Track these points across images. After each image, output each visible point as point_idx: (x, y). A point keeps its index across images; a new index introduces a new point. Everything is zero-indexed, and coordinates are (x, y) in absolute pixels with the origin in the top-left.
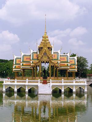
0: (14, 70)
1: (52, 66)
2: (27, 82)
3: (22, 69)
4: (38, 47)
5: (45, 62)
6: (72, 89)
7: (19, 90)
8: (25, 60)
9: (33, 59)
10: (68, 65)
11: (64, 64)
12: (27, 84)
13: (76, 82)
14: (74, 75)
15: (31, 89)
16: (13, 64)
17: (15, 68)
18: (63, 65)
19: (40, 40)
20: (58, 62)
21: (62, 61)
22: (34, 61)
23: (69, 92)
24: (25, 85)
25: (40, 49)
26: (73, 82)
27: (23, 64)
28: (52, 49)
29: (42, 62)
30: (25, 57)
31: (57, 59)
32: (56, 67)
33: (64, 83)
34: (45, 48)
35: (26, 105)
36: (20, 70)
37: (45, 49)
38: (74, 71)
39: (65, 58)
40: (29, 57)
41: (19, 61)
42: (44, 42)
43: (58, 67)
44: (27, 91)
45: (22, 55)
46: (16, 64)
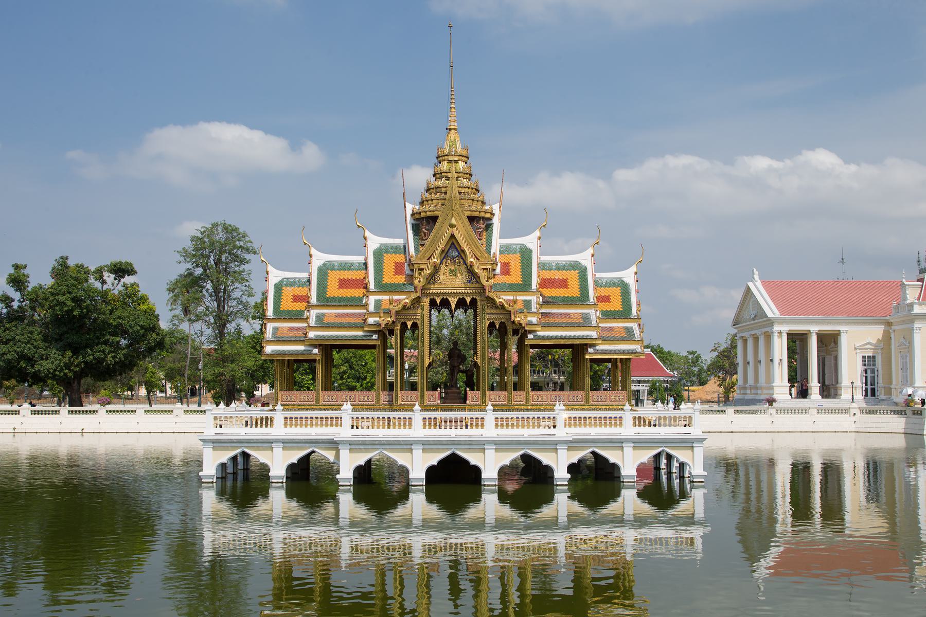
0: (269, 349)
2: (347, 422)
3: (375, 332)
4: (409, 212)
5: (453, 301)
7: (363, 474)
8: (333, 291)
11: (567, 315)
12: (344, 432)
13: (639, 421)
15: (369, 462)
18: (564, 320)
20: (528, 304)
21: (549, 292)
22: (386, 298)
23: (453, 480)
24: (336, 443)
25: (424, 224)
27: (319, 318)
28: (489, 227)
29: (433, 303)
30: (389, 262)
32: (515, 332)
33: (568, 430)
34: (454, 221)
35: (338, 562)
36: (361, 333)
39: (573, 277)
41: (297, 299)
43: (531, 332)
44: (350, 475)
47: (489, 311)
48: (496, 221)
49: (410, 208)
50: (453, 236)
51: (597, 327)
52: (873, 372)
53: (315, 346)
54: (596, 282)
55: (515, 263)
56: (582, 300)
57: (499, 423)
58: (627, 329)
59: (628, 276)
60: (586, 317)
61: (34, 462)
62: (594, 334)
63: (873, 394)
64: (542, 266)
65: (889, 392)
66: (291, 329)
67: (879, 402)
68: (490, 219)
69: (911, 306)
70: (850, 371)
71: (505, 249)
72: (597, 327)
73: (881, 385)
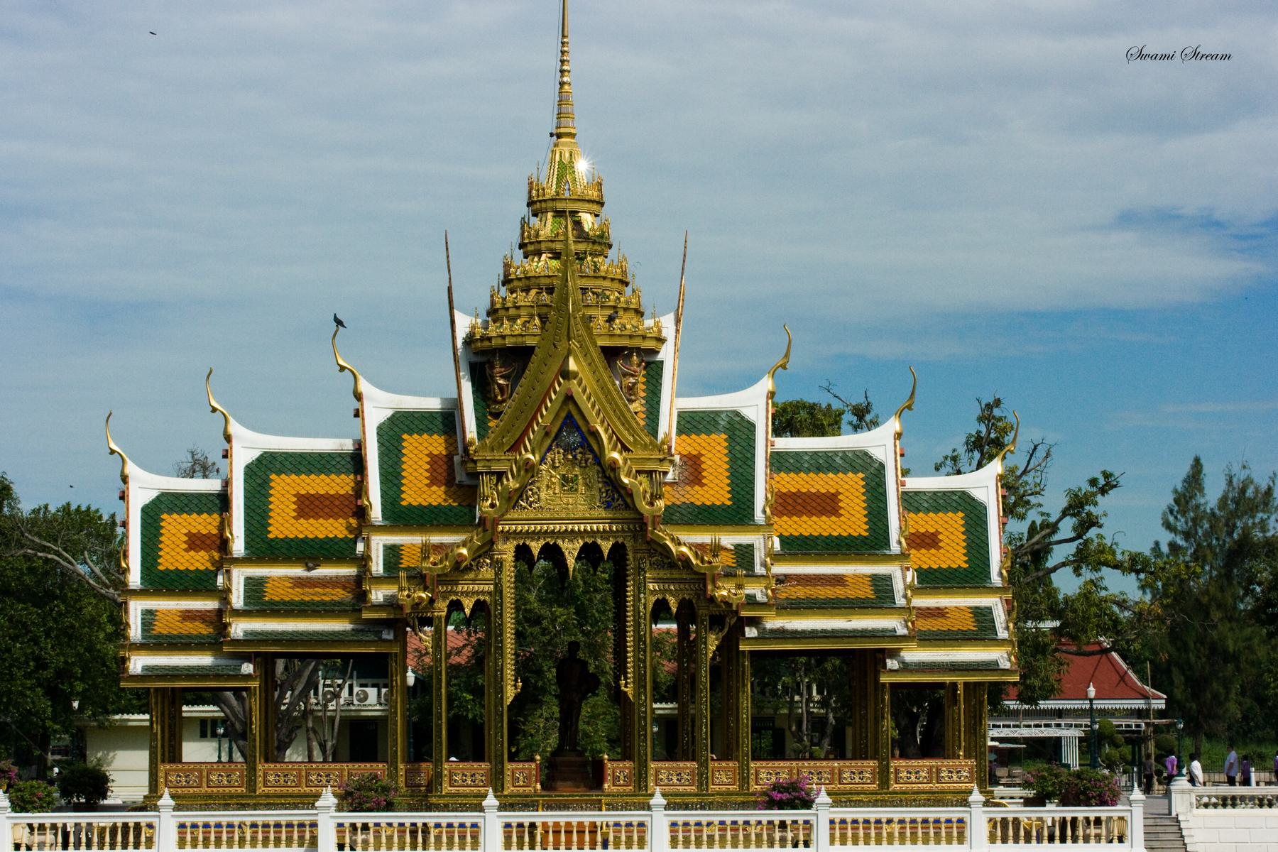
0: (137, 663)
8: (285, 523)
11: (838, 580)
16: (121, 585)
17: (155, 643)
22: (409, 540)
27: (255, 587)
28: (654, 371)
37: (543, 350)
39: (850, 487)
40: (340, 484)
41: (195, 541)
42: (543, 265)
43: (755, 622)
45: (243, 456)
46: (161, 582)
48: (666, 353)
49: (464, 325)
50: (569, 398)
53: (247, 658)
55: (714, 450)
60: (882, 586)
66: (188, 616)
71: (691, 423)
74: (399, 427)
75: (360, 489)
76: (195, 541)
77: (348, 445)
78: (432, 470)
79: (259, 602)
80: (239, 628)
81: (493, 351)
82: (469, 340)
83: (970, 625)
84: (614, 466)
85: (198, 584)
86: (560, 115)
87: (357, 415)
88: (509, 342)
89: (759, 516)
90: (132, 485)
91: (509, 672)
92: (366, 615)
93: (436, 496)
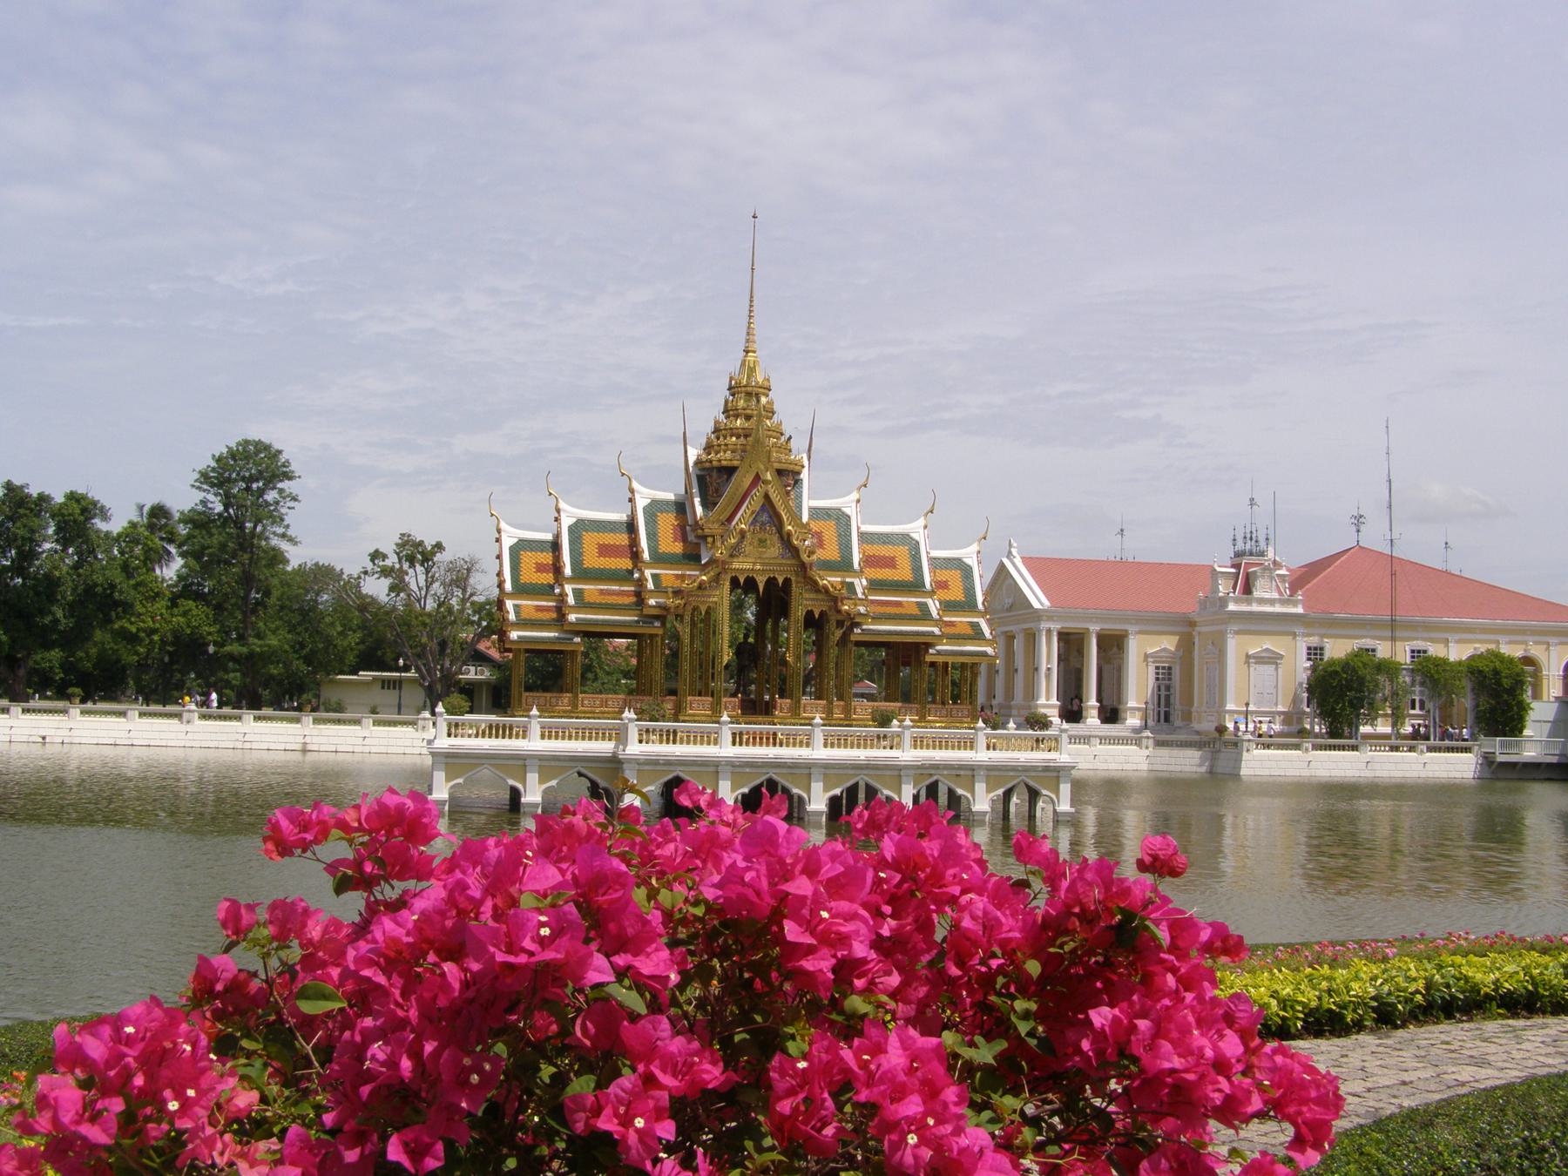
1: (810, 614)
6: (800, 798)
8: (592, 560)
9: (582, 574)
10: (923, 615)
11: (898, 604)
14: (484, 698)
17: (523, 623)
19: (706, 415)
22: (668, 573)
26: (970, 744)
30: (529, 559)
31: (844, 565)
32: (840, 624)
37: (740, 467)
38: (950, 660)
39: (901, 553)
41: (540, 568)
47: (807, 596)
48: (804, 475)
50: (767, 496)
51: (940, 620)
52: (1168, 688)
53: (577, 633)
54: (932, 560)
56: (915, 586)
57: (737, 739)
58: (971, 624)
59: (969, 555)
60: (923, 607)
61: (202, 768)
62: (936, 630)
63: (1167, 720)
64: (865, 537)
65: (1187, 716)
66: (539, 609)
67: (1175, 730)
68: (799, 473)
69: (1223, 602)
70: (1138, 689)
71: (816, 513)
72: (940, 620)
73: (1178, 706)
74: (654, 508)
75: (634, 542)
76: (540, 568)
77: (549, 537)
78: (675, 533)
79: (582, 603)
80: (572, 617)
81: (712, 469)
82: (698, 462)
83: (970, 631)
84: (789, 534)
85: (546, 591)
86: (747, 341)
87: (556, 520)
88: (724, 463)
89: (856, 566)
90: (637, 496)
91: (726, 646)
92: (645, 612)
93: (678, 548)
